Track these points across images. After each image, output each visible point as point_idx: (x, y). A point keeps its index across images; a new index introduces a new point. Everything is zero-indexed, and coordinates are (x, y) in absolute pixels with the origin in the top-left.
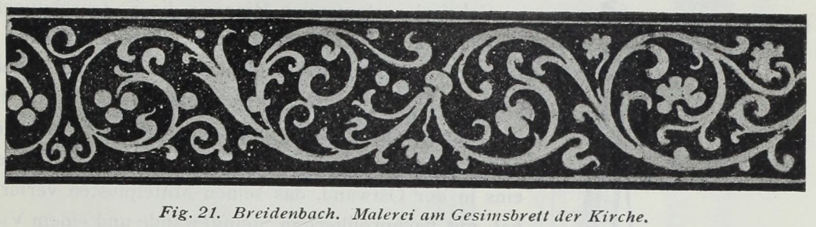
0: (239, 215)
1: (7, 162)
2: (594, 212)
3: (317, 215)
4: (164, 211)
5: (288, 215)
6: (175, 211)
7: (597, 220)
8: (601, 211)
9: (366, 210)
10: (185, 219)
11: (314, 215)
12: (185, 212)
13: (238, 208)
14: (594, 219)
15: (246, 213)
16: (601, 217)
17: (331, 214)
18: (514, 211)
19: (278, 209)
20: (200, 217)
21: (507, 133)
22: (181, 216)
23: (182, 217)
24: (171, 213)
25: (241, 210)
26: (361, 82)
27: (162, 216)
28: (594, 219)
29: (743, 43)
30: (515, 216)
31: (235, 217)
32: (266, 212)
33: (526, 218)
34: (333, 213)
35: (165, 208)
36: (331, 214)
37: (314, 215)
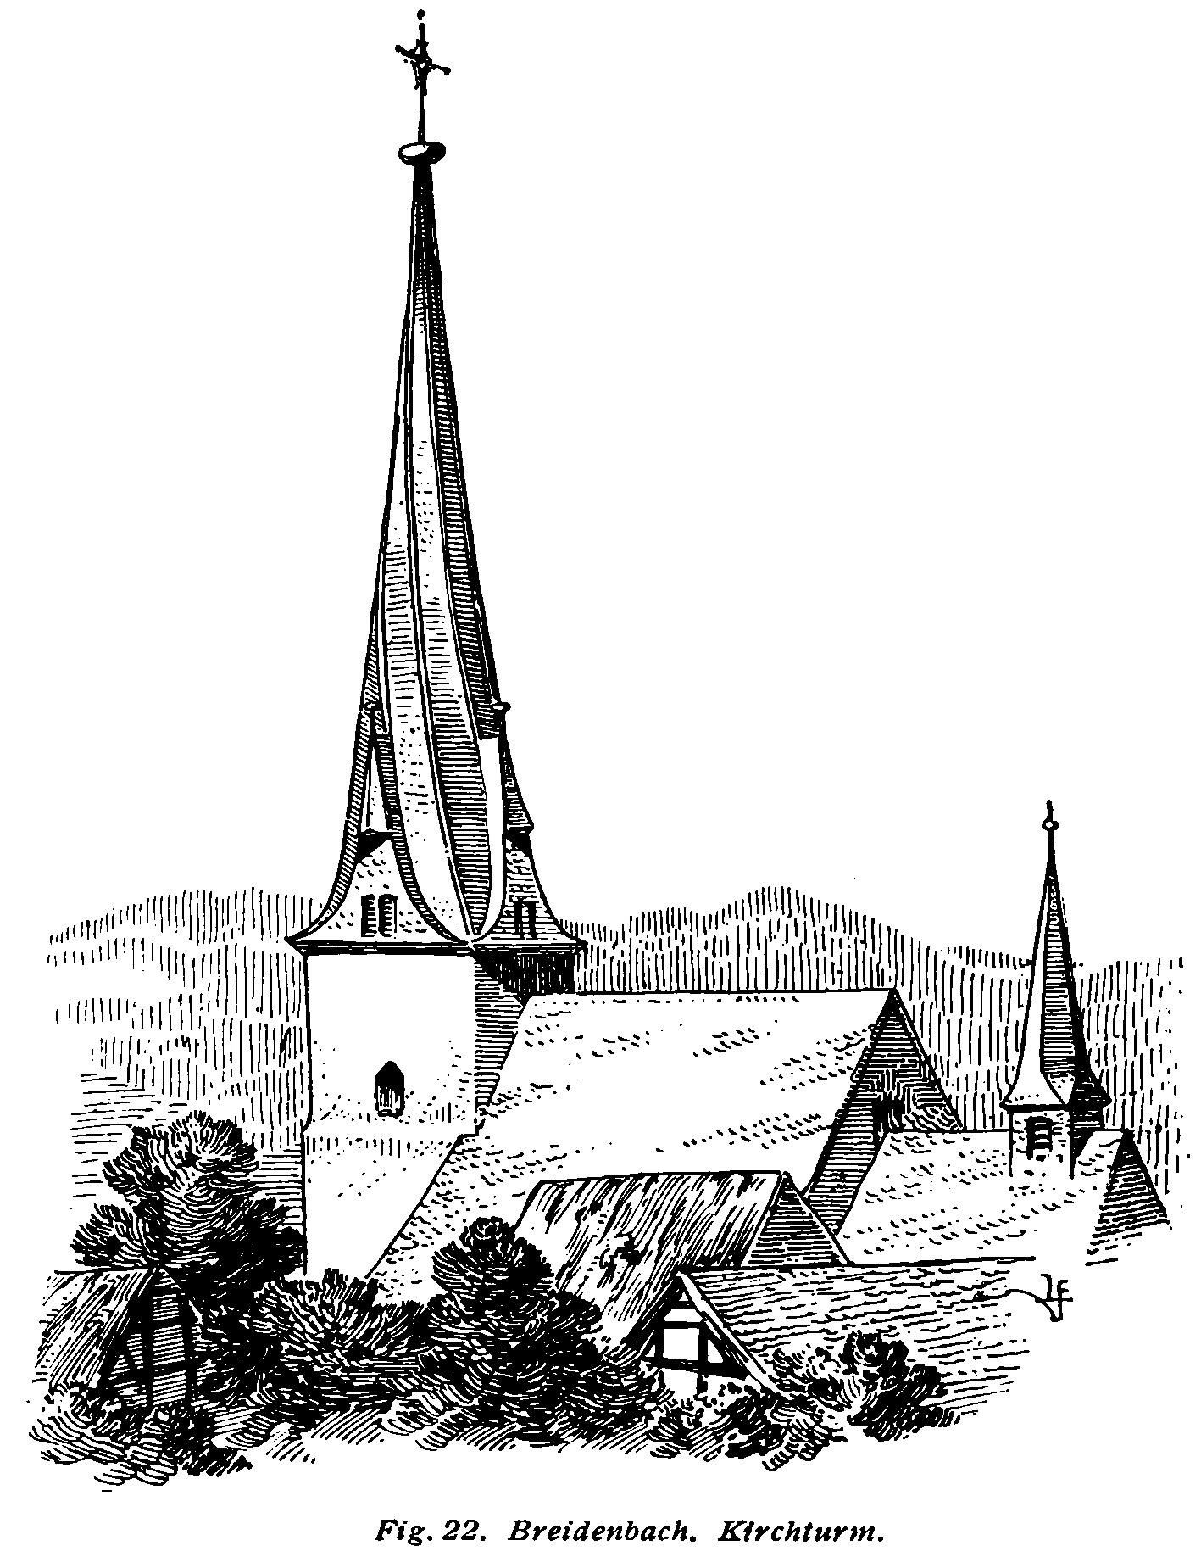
0: (520, 1534)
1: (193, 1447)
2: (728, 1523)
3: (656, 1533)
4: (382, 1529)
5: (606, 1533)
6: (401, 1529)
7: (735, 1538)
8: (740, 1523)
9: (809, 1527)
10: (420, 1542)
11: (650, 1534)
12: (421, 1530)
13: (518, 1523)
14: (729, 1536)
15: (531, 1532)
16: (740, 1532)
17: (681, 1532)
18: (631, 1523)
19: (588, 1523)
20: (446, 1537)
21: (668, 1318)
22: (412, 1536)
23: (414, 1539)
24: (395, 1531)
25: (523, 1526)
26: (1083, 1095)
27: (380, 1538)
28: (729, 1536)
29: (685, 930)
30: (632, 1532)
31: (513, 1538)
32: (567, 1529)
33: (545, 1534)
34: (685, 1529)
35: (384, 1522)
36: (681, 1532)
37: (650, 1534)
